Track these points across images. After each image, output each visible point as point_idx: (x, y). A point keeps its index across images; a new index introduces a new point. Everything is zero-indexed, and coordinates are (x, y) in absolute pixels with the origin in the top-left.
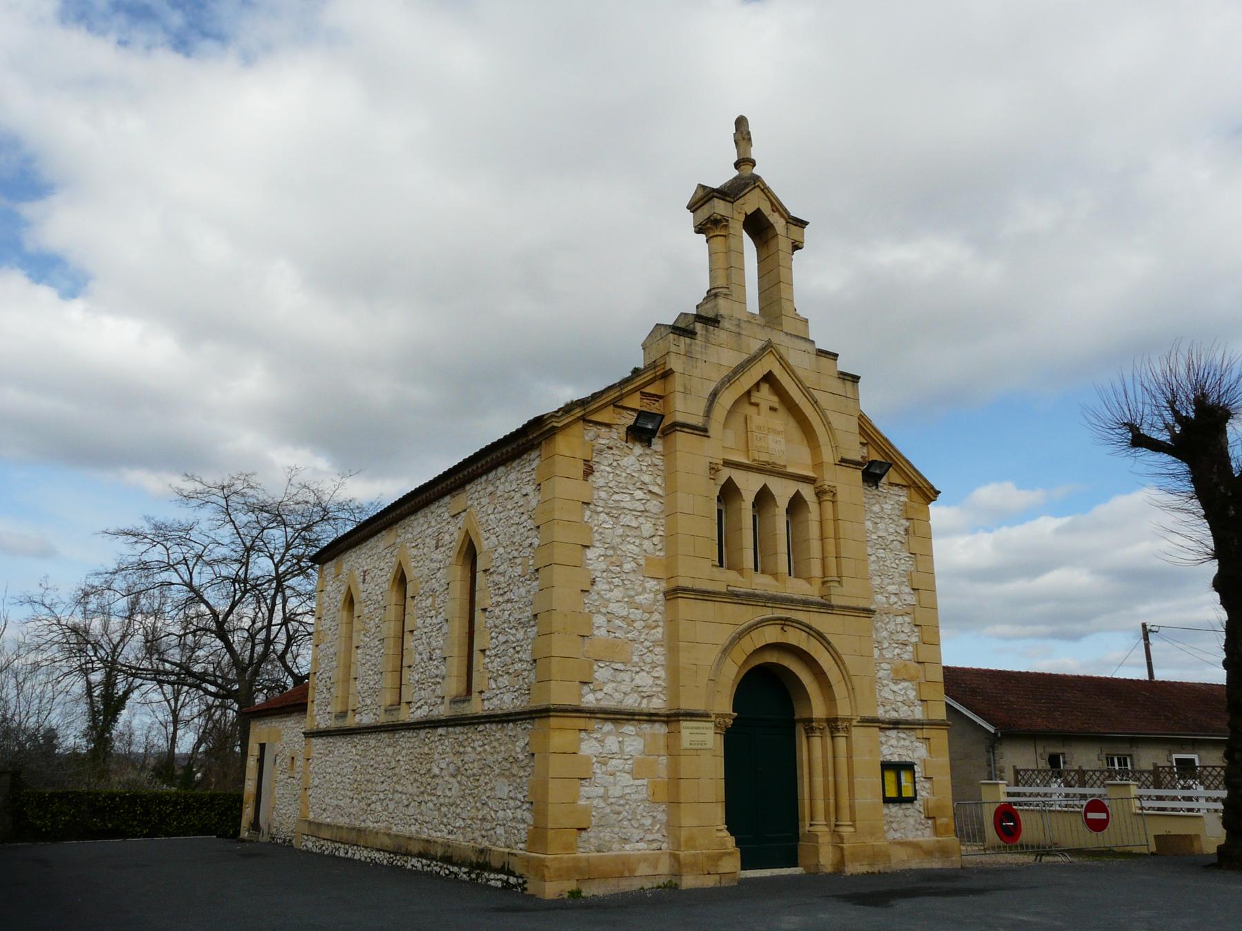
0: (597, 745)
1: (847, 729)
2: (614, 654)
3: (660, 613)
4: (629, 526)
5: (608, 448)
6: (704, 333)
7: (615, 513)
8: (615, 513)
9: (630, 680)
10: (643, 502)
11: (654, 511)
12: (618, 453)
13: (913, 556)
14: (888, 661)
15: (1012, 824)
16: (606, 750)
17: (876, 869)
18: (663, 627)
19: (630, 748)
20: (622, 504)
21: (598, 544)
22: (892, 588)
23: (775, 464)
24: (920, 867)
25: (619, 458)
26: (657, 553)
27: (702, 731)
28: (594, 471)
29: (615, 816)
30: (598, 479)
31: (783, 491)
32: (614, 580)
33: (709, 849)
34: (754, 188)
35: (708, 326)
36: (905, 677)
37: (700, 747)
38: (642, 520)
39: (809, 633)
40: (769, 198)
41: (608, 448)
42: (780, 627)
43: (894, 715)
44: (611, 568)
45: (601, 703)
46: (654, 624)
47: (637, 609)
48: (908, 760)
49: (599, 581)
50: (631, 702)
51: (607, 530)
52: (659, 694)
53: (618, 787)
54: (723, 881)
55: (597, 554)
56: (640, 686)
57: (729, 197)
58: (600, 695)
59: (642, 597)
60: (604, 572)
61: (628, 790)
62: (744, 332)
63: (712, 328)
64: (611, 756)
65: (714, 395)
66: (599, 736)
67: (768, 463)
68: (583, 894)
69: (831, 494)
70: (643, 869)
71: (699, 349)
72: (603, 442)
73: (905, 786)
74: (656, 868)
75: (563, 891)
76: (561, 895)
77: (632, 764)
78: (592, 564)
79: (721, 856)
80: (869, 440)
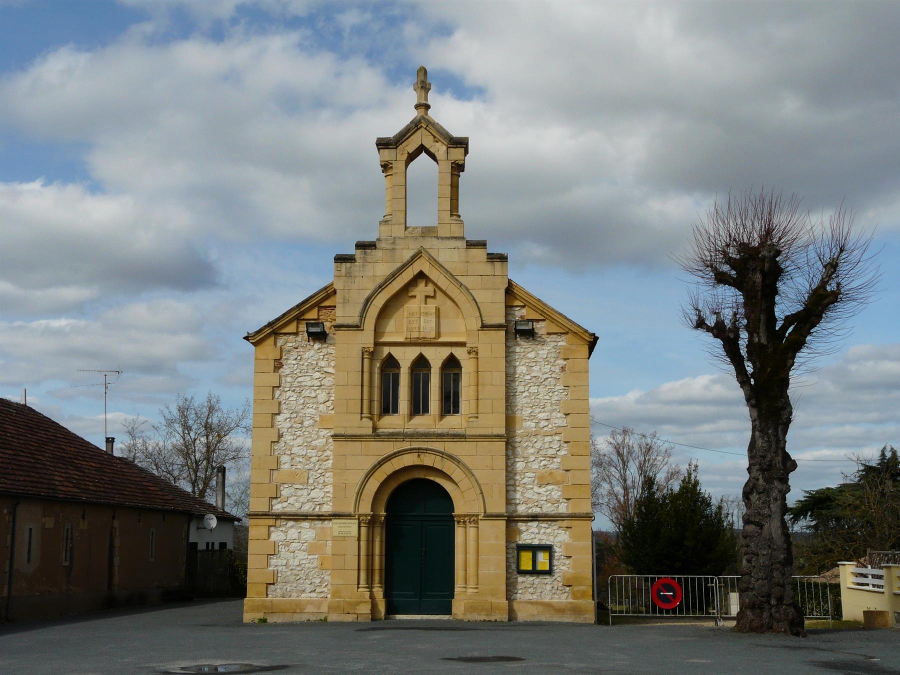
0: (282, 534)
1: (476, 522)
2: (300, 479)
3: (331, 451)
4: (309, 397)
5: (294, 348)
6: (363, 256)
7: (299, 390)
8: (299, 390)
9: (307, 494)
10: (320, 380)
11: (327, 385)
12: (302, 350)
13: (567, 388)
14: (534, 471)
15: (672, 594)
16: (289, 537)
17: (493, 618)
18: (333, 459)
19: (305, 537)
20: (304, 384)
21: (285, 411)
22: (541, 416)
23: (425, 338)
24: (551, 621)
25: (302, 353)
26: (330, 412)
27: (348, 525)
28: (283, 365)
29: (294, 577)
30: (285, 370)
31: (436, 357)
32: (296, 433)
33: (351, 598)
35: (366, 250)
36: (550, 482)
37: (346, 535)
38: (318, 392)
39: (442, 457)
40: (431, 133)
41: (294, 348)
42: (417, 454)
43: (537, 510)
44: (294, 425)
45: (286, 509)
46: (326, 458)
47: (313, 449)
48: (548, 543)
49: (286, 435)
50: (307, 508)
51: (293, 402)
52: (329, 503)
53: (296, 560)
54: (359, 618)
55: (285, 417)
56: (314, 498)
57: (392, 145)
58: (285, 504)
59: (317, 442)
60: (289, 428)
61: (304, 562)
64: (292, 541)
65: (368, 301)
66: (284, 529)
67: (418, 338)
68: (268, 621)
69: (474, 353)
70: (310, 609)
71: (358, 269)
72: (291, 345)
73: (542, 563)
74: (319, 608)
75: (254, 618)
76: (253, 621)
77: (307, 546)
78: (281, 424)
79: (358, 603)
80: (526, 303)
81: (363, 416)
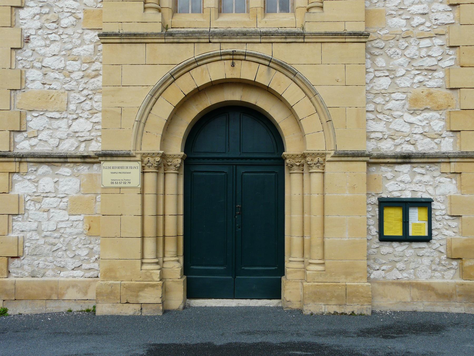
81: (147, 5)
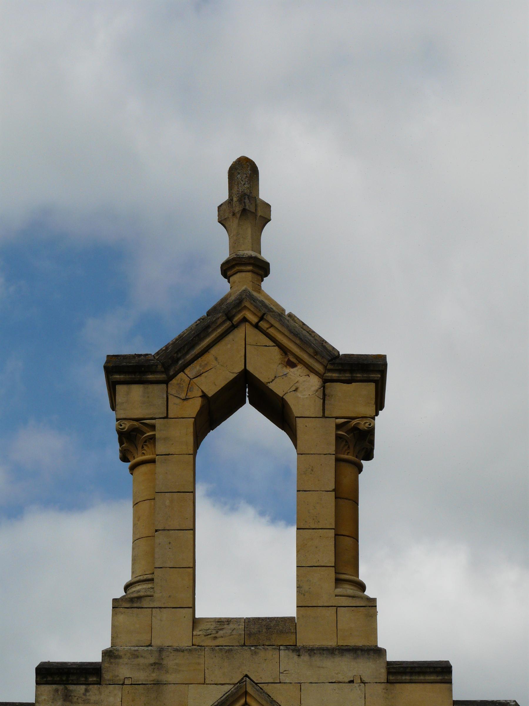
34: (234, 327)
62: (170, 678)
63: (83, 687)
